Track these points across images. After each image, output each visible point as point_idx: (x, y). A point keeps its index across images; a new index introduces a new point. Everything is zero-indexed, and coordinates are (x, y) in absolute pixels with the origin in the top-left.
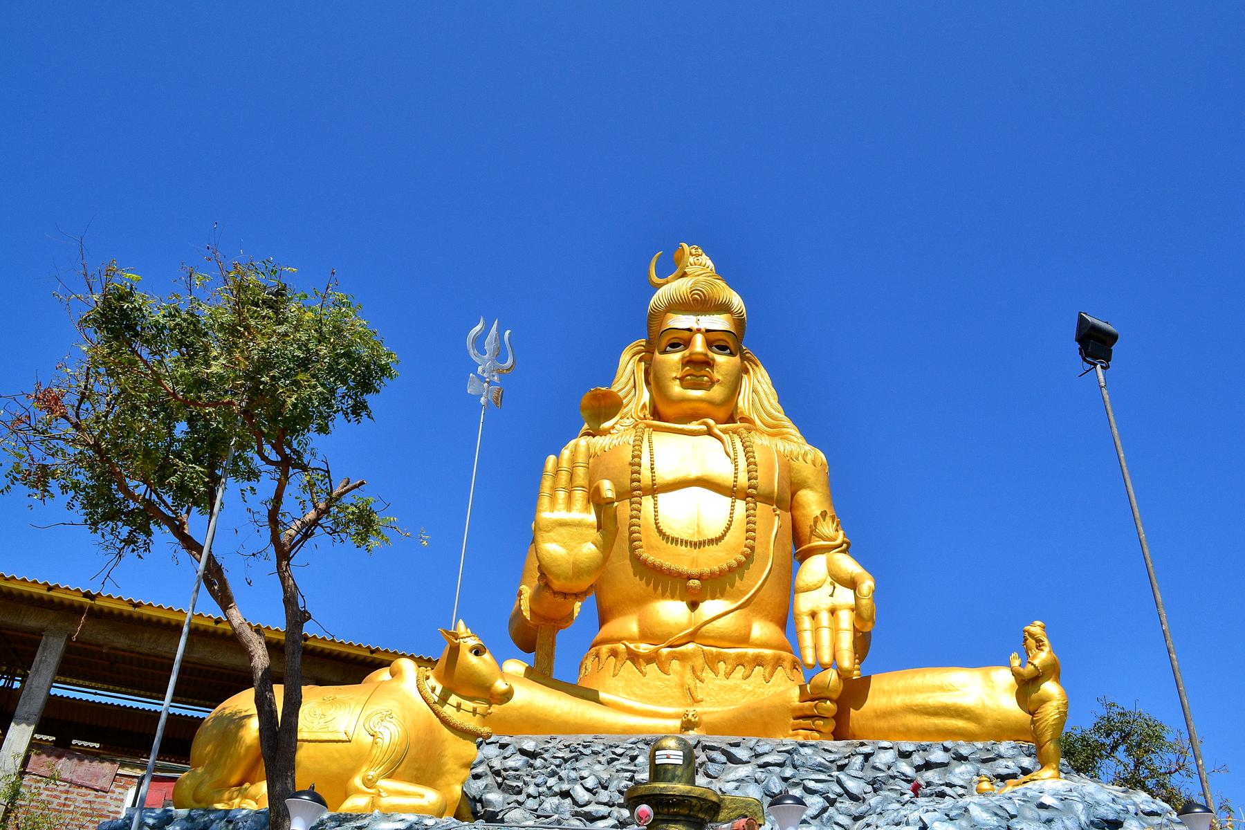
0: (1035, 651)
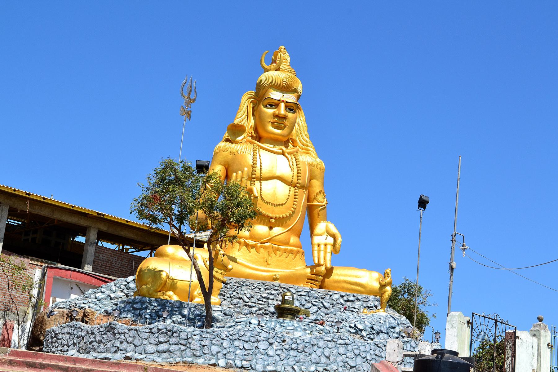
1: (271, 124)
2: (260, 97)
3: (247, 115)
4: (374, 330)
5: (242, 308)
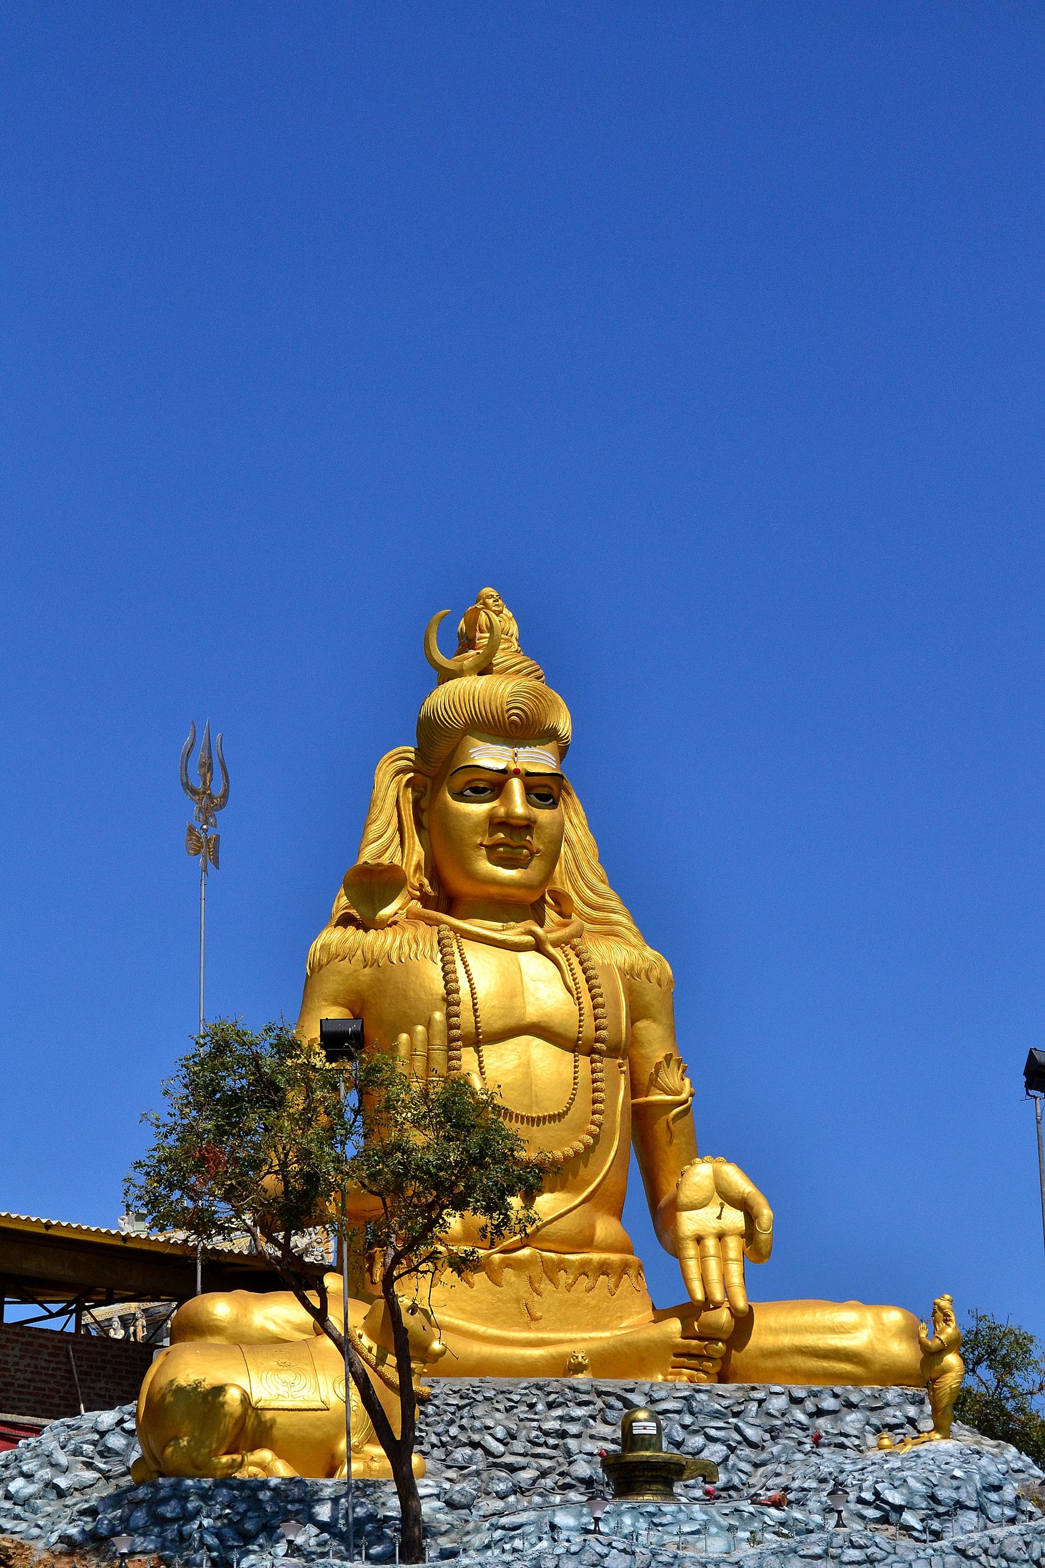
0: (942, 1324)
1: (484, 851)
2: (437, 764)
3: (401, 829)
4: (938, 1502)
5: (485, 1476)
